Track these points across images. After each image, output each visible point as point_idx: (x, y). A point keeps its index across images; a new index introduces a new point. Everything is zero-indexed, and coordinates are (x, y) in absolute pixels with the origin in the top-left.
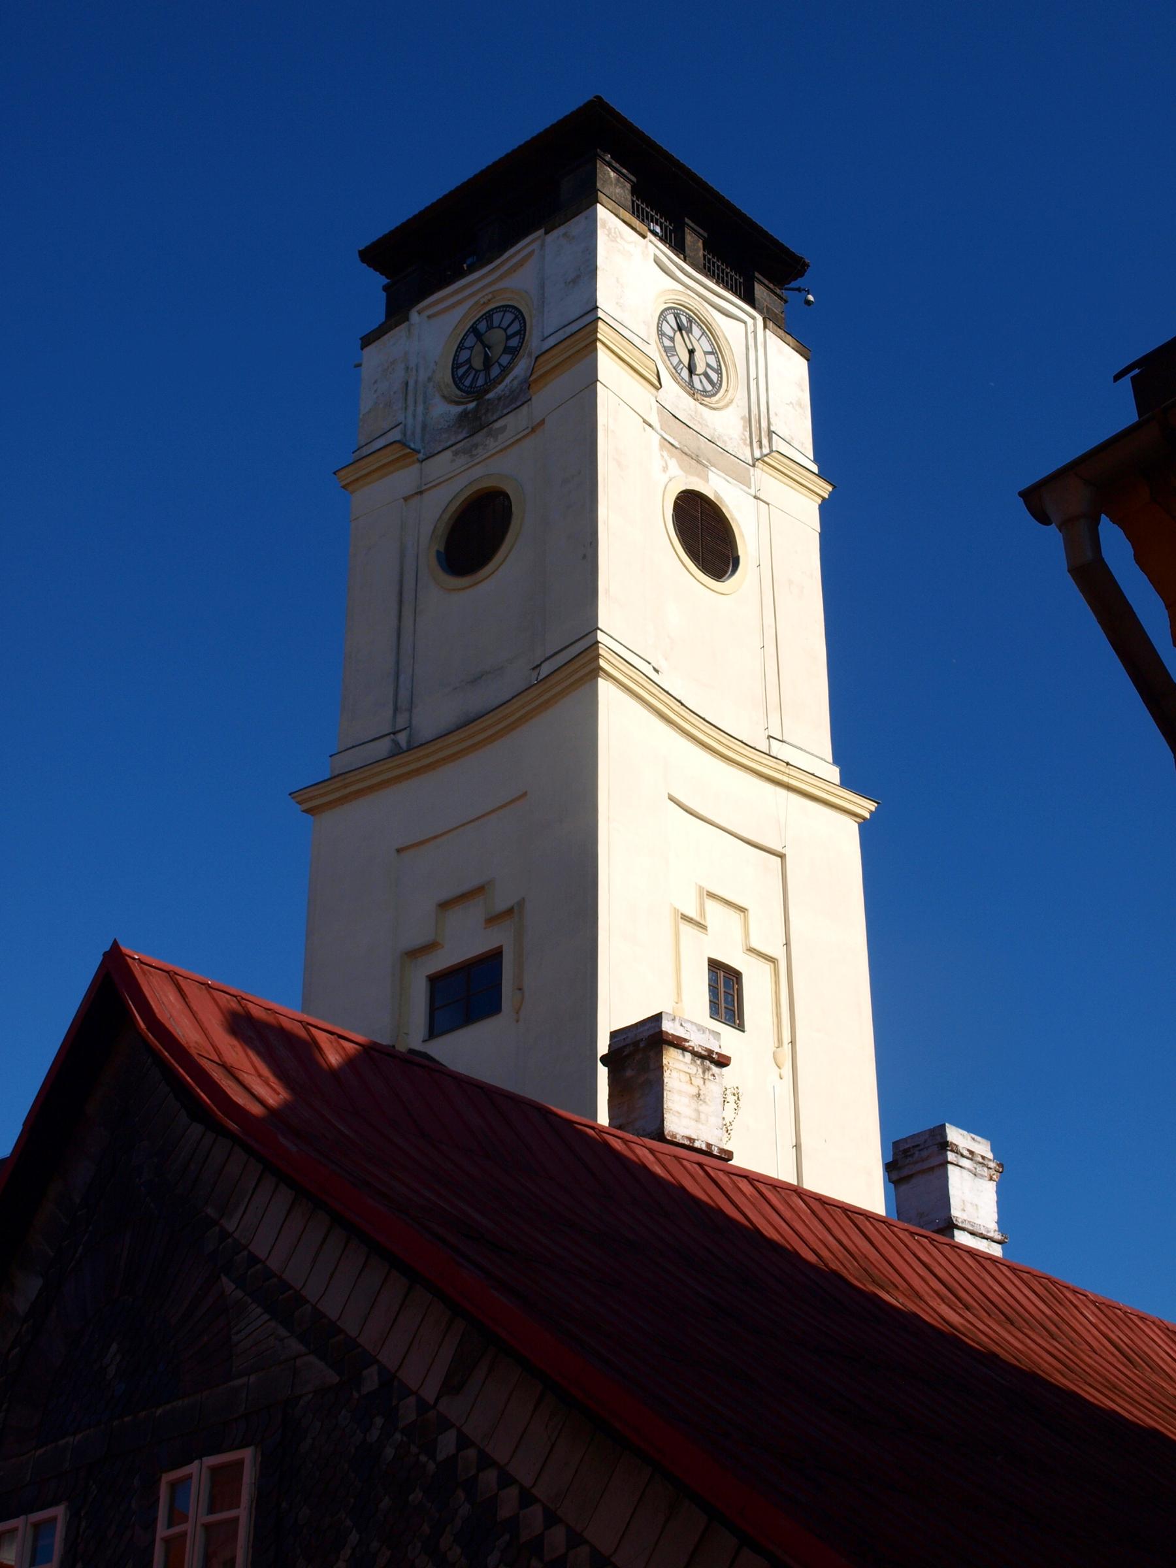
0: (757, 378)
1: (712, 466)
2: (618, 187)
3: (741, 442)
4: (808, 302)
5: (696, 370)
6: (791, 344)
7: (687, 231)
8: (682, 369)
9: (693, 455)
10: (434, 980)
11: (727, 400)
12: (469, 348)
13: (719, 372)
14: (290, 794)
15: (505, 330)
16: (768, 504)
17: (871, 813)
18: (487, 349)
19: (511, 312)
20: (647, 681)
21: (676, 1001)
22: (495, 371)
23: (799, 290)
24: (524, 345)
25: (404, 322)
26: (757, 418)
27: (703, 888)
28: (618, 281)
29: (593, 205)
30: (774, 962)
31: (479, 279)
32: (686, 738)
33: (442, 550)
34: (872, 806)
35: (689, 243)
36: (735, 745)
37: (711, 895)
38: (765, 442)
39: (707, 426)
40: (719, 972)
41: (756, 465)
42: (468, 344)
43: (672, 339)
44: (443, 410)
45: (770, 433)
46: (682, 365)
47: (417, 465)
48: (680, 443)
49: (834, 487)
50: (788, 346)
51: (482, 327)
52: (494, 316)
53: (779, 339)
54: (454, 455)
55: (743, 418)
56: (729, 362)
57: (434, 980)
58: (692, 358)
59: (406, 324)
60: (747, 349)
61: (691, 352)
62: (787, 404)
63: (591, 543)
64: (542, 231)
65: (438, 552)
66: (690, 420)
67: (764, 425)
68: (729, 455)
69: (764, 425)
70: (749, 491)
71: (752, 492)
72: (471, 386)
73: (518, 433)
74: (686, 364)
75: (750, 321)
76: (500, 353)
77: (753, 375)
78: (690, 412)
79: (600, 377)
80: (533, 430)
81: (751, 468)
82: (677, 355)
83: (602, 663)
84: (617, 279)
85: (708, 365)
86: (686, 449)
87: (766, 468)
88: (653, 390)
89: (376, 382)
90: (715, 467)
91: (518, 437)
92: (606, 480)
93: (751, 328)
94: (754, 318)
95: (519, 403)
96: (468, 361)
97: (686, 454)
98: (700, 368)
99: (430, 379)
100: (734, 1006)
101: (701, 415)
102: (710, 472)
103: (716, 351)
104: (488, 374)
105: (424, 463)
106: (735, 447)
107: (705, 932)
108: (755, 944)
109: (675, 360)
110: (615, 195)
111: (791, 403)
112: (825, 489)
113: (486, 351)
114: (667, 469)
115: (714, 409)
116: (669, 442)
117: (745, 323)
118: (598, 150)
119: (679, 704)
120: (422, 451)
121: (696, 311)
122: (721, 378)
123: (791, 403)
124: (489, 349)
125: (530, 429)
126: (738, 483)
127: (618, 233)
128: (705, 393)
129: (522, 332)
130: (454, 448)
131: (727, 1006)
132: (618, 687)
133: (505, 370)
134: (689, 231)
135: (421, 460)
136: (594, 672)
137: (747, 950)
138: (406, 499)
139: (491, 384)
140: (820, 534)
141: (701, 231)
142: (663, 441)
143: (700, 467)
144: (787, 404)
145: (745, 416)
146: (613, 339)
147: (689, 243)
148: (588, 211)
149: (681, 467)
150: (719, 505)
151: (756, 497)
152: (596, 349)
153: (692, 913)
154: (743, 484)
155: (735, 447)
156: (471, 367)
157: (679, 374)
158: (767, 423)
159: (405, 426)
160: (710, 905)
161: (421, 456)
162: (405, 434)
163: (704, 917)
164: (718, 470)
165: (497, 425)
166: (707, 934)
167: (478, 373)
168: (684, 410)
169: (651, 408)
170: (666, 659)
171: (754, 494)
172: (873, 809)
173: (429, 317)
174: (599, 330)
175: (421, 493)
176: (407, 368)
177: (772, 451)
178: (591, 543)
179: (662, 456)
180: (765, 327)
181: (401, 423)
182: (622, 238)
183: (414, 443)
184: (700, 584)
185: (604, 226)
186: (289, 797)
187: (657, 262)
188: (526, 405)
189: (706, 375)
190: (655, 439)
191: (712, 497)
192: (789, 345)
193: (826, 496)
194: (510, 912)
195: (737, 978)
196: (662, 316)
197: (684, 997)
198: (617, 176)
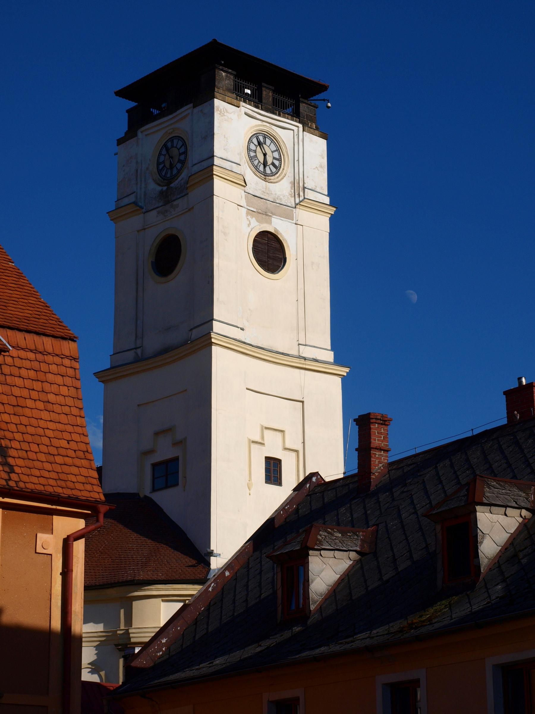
0: (298, 160)
1: (273, 215)
2: (227, 80)
3: (289, 197)
4: (329, 107)
5: (267, 163)
6: (317, 135)
7: (264, 89)
8: (260, 166)
9: (264, 213)
10: (154, 466)
11: (283, 175)
12: (164, 155)
13: (279, 160)
14: (94, 374)
15: (179, 150)
16: (302, 226)
17: (347, 373)
18: (171, 159)
19: (182, 141)
20: (235, 342)
21: (249, 480)
22: (175, 171)
23: (324, 100)
24: (186, 162)
25: (135, 137)
26: (298, 181)
27: (263, 426)
28: (225, 137)
29: (213, 99)
30: (297, 452)
31: (167, 121)
32: (256, 359)
33: (154, 261)
34: (347, 370)
35: (264, 96)
36: (279, 357)
37: (267, 428)
38: (301, 194)
39: (272, 194)
40: (270, 461)
41: (296, 207)
42: (161, 160)
43: (255, 151)
44: (153, 187)
45: (304, 188)
46: (260, 163)
47: (142, 215)
48: (257, 209)
49: (337, 208)
50: (315, 136)
51: (169, 144)
52: (174, 140)
53: (311, 135)
54: (157, 214)
55: (291, 183)
56: (284, 151)
57: (154, 466)
58: (265, 158)
59: (135, 139)
60: (294, 144)
61: (265, 155)
62: (314, 169)
63: (211, 276)
64: (191, 105)
65: (152, 262)
66: (263, 194)
67: (301, 185)
68: (282, 206)
69: (301, 185)
70: (293, 222)
71: (294, 222)
72: (165, 176)
73: (184, 210)
74: (262, 162)
75: (295, 129)
76: (176, 162)
77: (296, 159)
78: (263, 190)
79: (215, 193)
80: (189, 210)
81: (294, 209)
82: (258, 159)
83: (213, 340)
84: (224, 136)
85: (274, 158)
86: (260, 211)
87: (301, 207)
88: (243, 188)
89: (124, 166)
90: (275, 215)
91: (183, 212)
92: (218, 244)
93: (296, 133)
94: (298, 127)
95: (184, 194)
96: (164, 162)
97: (260, 213)
98: (270, 160)
99: (147, 169)
100: (278, 475)
101: (269, 188)
102: (272, 218)
103: (278, 150)
104: (172, 173)
105: (145, 214)
106: (286, 200)
107: (264, 446)
108: (288, 446)
109: (256, 163)
110: (225, 85)
111: (317, 167)
112: (332, 210)
113: (170, 160)
114: (250, 224)
115: (275, 183)
116: (251, 211)
117: (293, 130)
118: (216, 65)
119: (251, 347)
120: (144, 207)
121: (268, 132)
122: (281, 163)
123: (317, 167)
124: (172, 159)
125: (187, 210)
126: (287, 220)
127: (225, 111)
128: (273, 174)
129: (186, 153)
130: (158, 210)
131: (274, 475)
132: (221, 348)
133: (179, 171)
134: (264, 89)
135: (144, 212)
136: (210, 344)
137: (284, 449)
138: (138, 231)
139: (174, 178)
140: (329, 233)
141: (271, 87)
142: (248, 211)
143: (267, 217)
144: (314, 169)
145: (292, 181)
146: (220, 171)
147: (264, 96)
148: (210, 101)
149: (257, 221)
150: (277, 234)
151: (296, 224)
152: (213, 179)
153: (258, 439)
154: (289, 219)
155: (286, 200)
156: (164, 166)
157: (258, 169)
158: (303, 183)
159: (137, 193)
160: (266, 432)
161: (144, 210)
162: (136, 197)
163: (263, 440)
164: (277, 216)
165: (175, 203)
166: (265, 446)
167: (168, 170)
168: (260, 190)
169: (242, 197)
170: (248, 321)
171: (295, 223)
172: (348, 371)
173: (146, 135)
174: (214, 170)
175: (144, 229)
176: (137, 162)
177: (305, 198)
178: (211, 276)
179: (248, 219)
180: (303, 131)
181: (135, 192)
182: (227, 112)
183: (141, 203)
184: (266, 278)
185: (218, 110)
186: (93, 375)
187: (246, 114)
188: (186, 196)
189: (273, 164)
190: (244, 211)
191: (273, 231)
192: (316, 136)
193: (333, 213)
194: (181, 442)
195: (279, 462)
196: (250, 141)
197: (253, 478)
198: (226, 74)
